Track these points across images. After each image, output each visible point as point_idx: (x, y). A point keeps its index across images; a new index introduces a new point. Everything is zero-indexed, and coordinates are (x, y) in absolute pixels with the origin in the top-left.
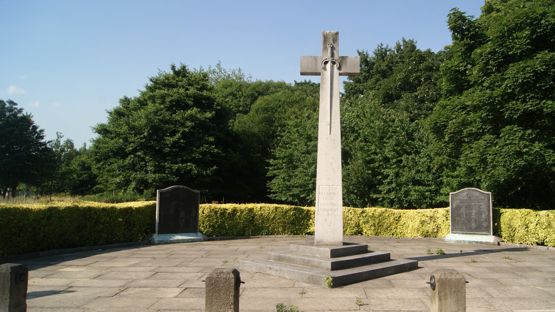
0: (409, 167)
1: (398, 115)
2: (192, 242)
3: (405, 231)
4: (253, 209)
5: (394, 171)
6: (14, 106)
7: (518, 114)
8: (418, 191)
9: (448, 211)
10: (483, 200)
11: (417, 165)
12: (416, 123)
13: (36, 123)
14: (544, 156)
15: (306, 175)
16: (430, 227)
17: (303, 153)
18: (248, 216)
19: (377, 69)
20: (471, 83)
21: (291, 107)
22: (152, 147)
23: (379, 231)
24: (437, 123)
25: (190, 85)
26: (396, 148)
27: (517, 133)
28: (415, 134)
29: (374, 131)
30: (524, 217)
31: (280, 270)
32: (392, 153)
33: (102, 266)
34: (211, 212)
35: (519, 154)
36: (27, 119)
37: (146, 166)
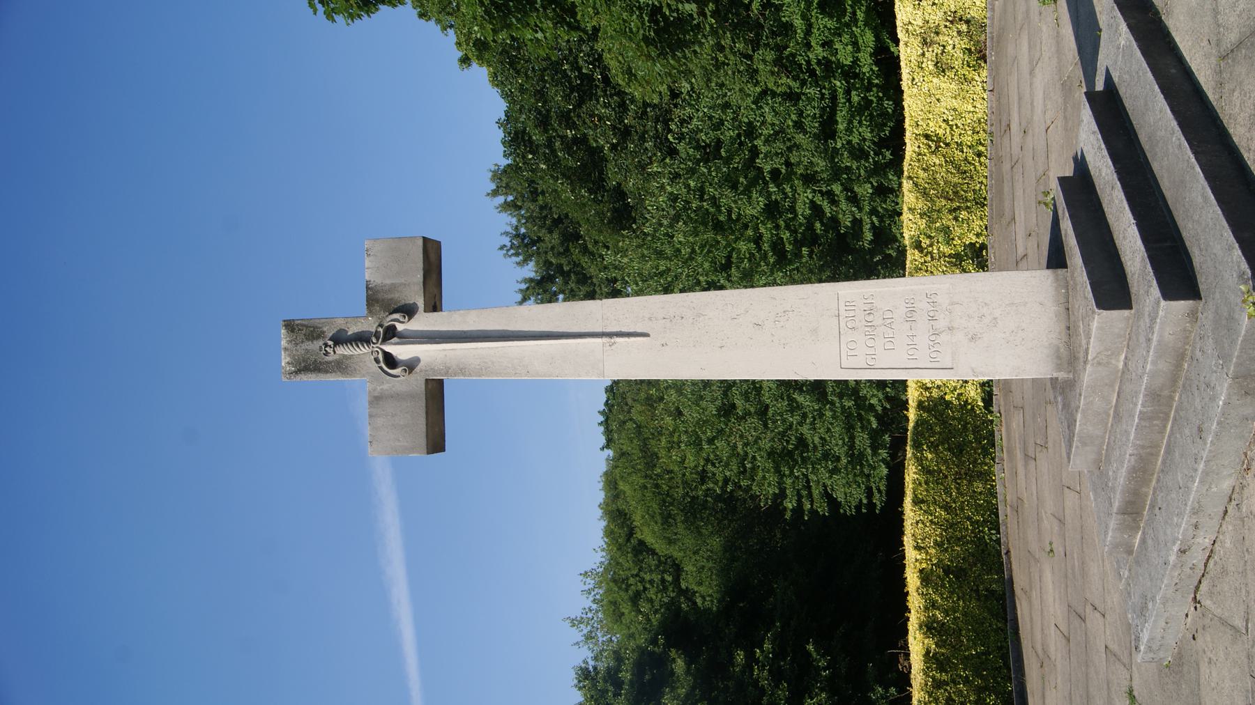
0: (790, 149)
4: (921, 571)
8: (850, 122)
11: (782, 131)
15: (821, 415)
16: (954, 44)
17: (765, 425)
18: (943, 586)
19: (560, 254)
24: (646, 39)
29: (702, 247)
31: (1195, 512)
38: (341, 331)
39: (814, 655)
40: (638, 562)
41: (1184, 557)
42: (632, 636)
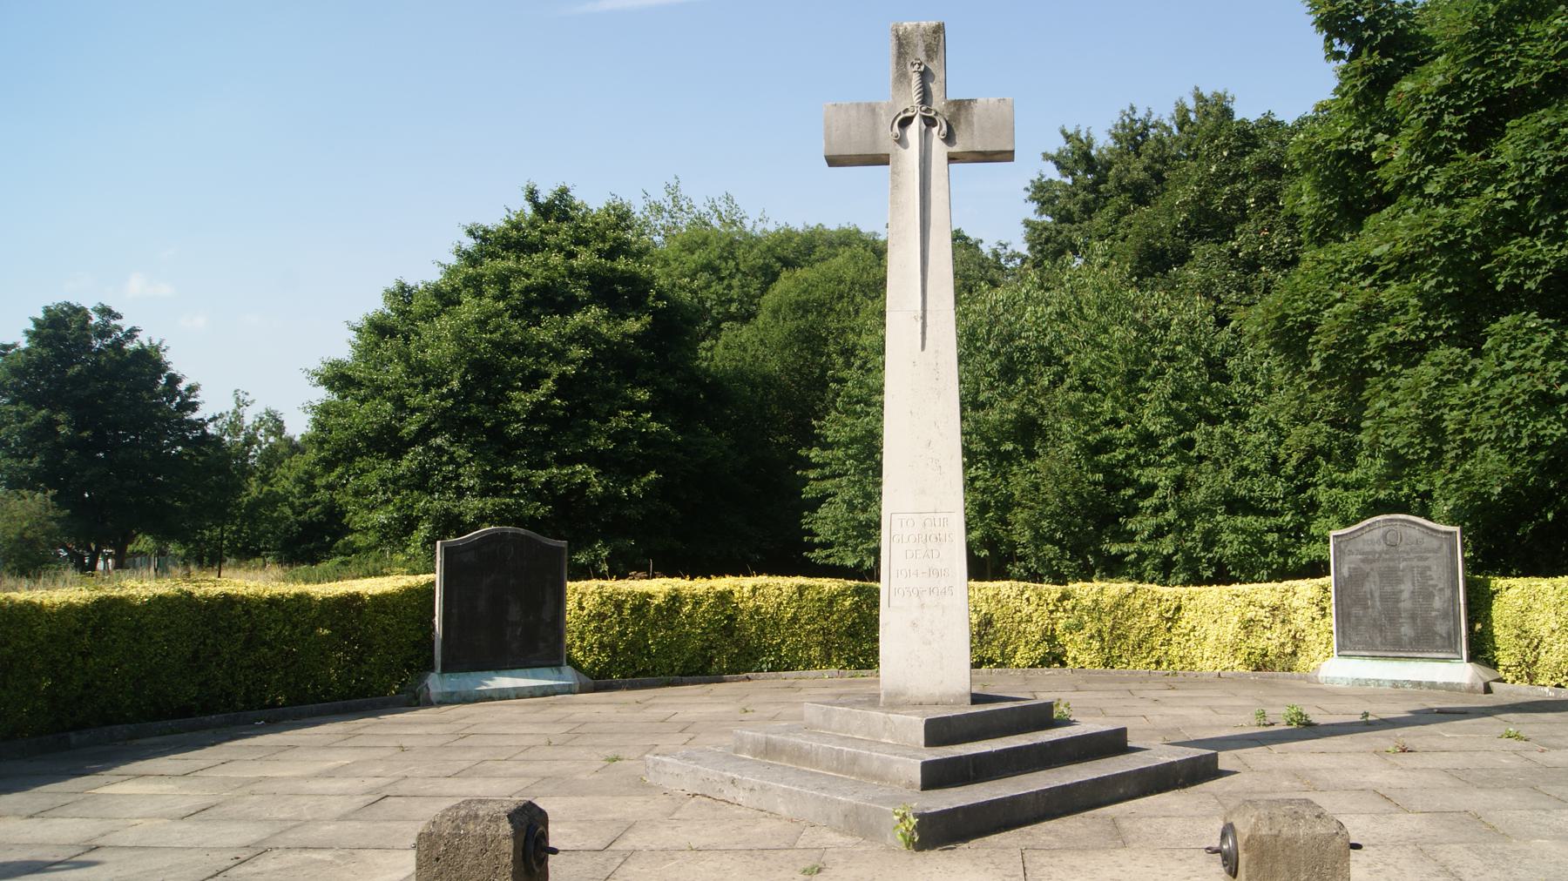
1: (1178, 308)
2: (544, 695)
4: (731, 592)
5: (1171, 472)
6: (113, 322)
7: (1539, 278)
8: (1244, 531)
9: (1326, 590)
10: (1435, 551)
11: (1238, 453)
13: (175, 369)
16: (1272, 640)
18: (716, 613)
19: (1120, 180)
20: (1386, 189)
21: (872, 299)
22: (474, 422)
23: (1116, 652)
24: (1285, 317)
26: (1174, 405)
27: (1538, 337)
28: (1231, 363)
29: (1108, 358)
31: (762, 787)
32: (1165, 420)
34: (603, 604)
37: (458, 476)
38: (933, 76)
39: (645, 480)
40: (753, 271)
42: (666, 263)
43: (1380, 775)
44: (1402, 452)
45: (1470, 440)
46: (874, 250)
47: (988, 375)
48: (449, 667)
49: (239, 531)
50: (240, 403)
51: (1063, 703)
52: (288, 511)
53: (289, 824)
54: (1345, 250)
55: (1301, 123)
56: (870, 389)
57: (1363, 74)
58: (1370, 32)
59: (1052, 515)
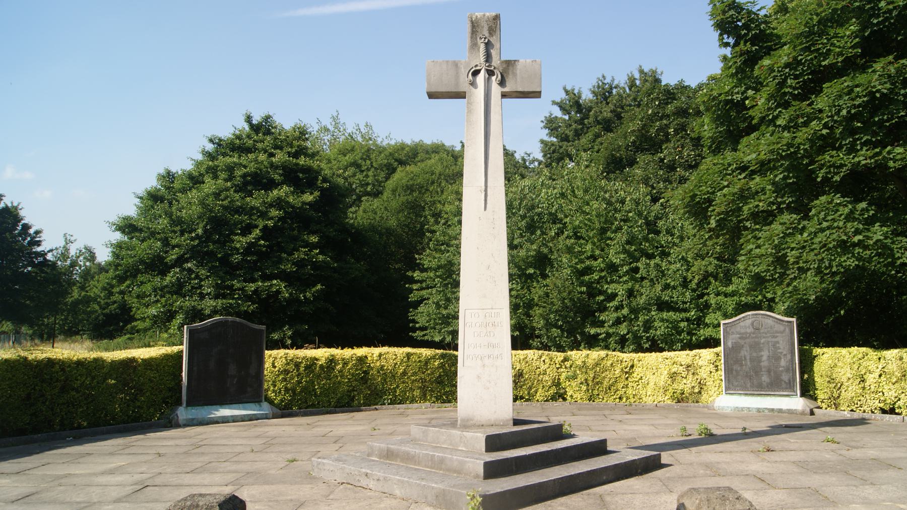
1: (629, 191)
3: (643, 392)
4: (366, 357)
5: (625, 286)
7: (842, 174)
8: (667, 321)
9: (718, 355)
10: (782, 332)
11: (664, 275)
12: (662, 205)
14: (892, 250)
16: (687, 384)
18: (357, 370)
19: (596, 117)
20: (754, 122)
21: (451, 184)
22: (211, 254)
23: (596, 392)
25: (276, 147)
26: (627, 247)
27: (841, 208)
28: (660, 223)
29: (589, 220)
30: (857, 363)
31: (385, 478)
32: (622, 256)
33: (48, 473)
34: (288, 364)
35: (845, 246)
36: (11, 212)
37: (201, 287)
38: (493, 46)
39: (314, 289)
41: (364, 476)
42: (329, 161)
43: (756, 466)
44: (763, 275)
45: (803, 268)
46: (452, 156)
47: (519, 229)
48: (191, 403)
49: (66, 319)
50: (68, 242)
51: (567, 424)
52: (97, 307)
53: (83, 505)
54: (729, 156)
55: (700, 87)
56: (450, 237)
57: (741, 56)
58: (745, 31)
59: (556, 311)
